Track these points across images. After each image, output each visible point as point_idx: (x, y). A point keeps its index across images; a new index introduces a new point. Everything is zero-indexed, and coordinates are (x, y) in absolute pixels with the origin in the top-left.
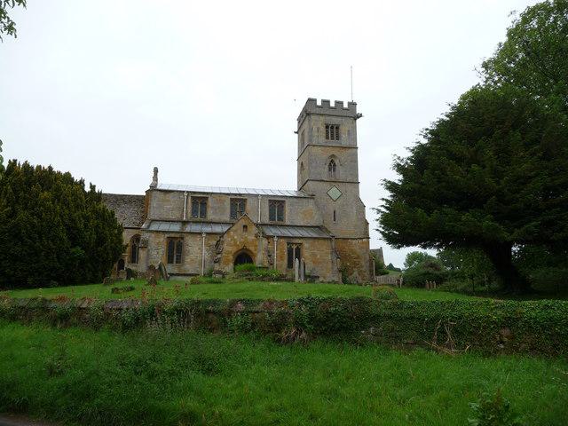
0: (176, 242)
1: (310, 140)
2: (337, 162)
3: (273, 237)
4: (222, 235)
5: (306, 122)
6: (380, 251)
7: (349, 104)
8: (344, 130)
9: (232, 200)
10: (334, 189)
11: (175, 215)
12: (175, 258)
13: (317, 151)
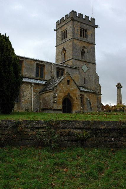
2: (86, 50)
8: (89, 32)
9: (37, 64)
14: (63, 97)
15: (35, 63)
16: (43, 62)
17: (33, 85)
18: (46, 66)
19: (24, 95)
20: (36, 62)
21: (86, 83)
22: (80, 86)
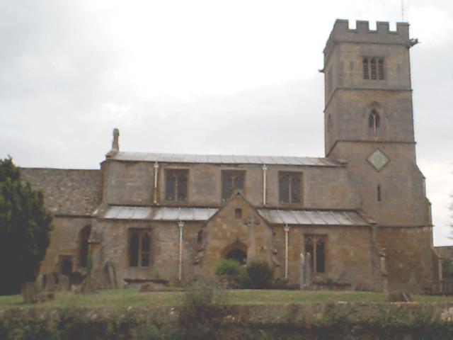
1: (340, 82)
2: (381, 112)
7: (399, 25)
8: (391, 64)
9: (224, 173)
16: (240, 166)
17: (181, 225)
18: (247, 173)
19: (160, 249)
21: (383, 197)
22: (260, 208)
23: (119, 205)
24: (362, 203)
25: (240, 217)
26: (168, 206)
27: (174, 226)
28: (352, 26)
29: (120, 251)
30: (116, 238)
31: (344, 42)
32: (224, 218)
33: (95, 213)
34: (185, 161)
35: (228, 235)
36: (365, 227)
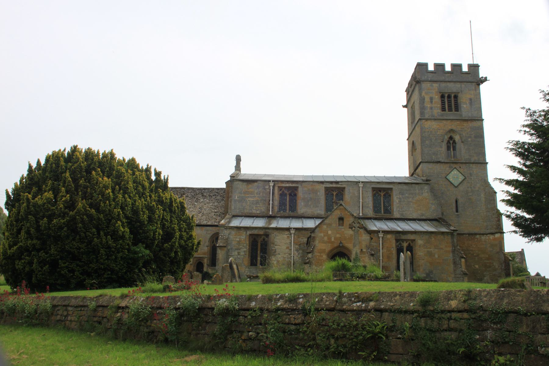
0: (260, 240)
1: (422, 113)
2: (457, 138)
3: (377, 232)
4: (312, 230)
5: (416, 92)
6: (521, 254)
7: (470, 66)
8: (464, 99)
9: (327, 189)
10: (455, 172)
11: (260, 209)
12: (259, 258)
13: (434, 125)
14: (327, 251)
15: (322, 188)
16: (340, 183)
17: (293, 232)
18: (346, 190)
19: (275, 252)
20: (324, 186)
23: (242, 216)
24: (442, 214)
25: (343, 225)
26: (282, 217)
27: (287, 233)
28: (431, 68)
29: (242, 253)
30: (239, 242)
31: (423, 81)
32: (329, 225)
33: (223, 222)
34: (295, 179)
35: (333, 240)
36: (447, 233)
